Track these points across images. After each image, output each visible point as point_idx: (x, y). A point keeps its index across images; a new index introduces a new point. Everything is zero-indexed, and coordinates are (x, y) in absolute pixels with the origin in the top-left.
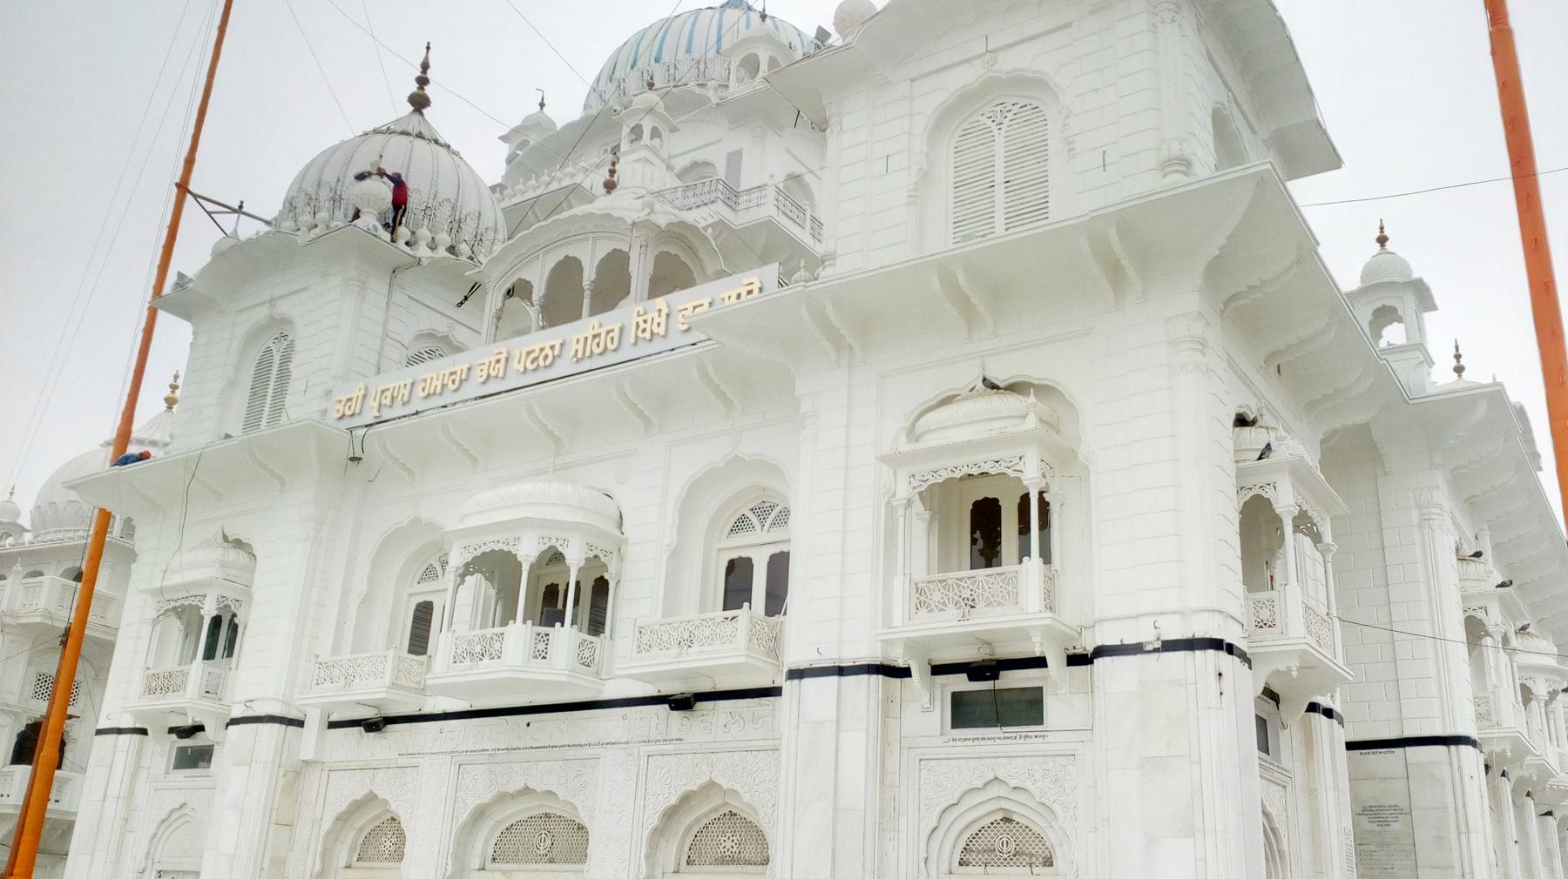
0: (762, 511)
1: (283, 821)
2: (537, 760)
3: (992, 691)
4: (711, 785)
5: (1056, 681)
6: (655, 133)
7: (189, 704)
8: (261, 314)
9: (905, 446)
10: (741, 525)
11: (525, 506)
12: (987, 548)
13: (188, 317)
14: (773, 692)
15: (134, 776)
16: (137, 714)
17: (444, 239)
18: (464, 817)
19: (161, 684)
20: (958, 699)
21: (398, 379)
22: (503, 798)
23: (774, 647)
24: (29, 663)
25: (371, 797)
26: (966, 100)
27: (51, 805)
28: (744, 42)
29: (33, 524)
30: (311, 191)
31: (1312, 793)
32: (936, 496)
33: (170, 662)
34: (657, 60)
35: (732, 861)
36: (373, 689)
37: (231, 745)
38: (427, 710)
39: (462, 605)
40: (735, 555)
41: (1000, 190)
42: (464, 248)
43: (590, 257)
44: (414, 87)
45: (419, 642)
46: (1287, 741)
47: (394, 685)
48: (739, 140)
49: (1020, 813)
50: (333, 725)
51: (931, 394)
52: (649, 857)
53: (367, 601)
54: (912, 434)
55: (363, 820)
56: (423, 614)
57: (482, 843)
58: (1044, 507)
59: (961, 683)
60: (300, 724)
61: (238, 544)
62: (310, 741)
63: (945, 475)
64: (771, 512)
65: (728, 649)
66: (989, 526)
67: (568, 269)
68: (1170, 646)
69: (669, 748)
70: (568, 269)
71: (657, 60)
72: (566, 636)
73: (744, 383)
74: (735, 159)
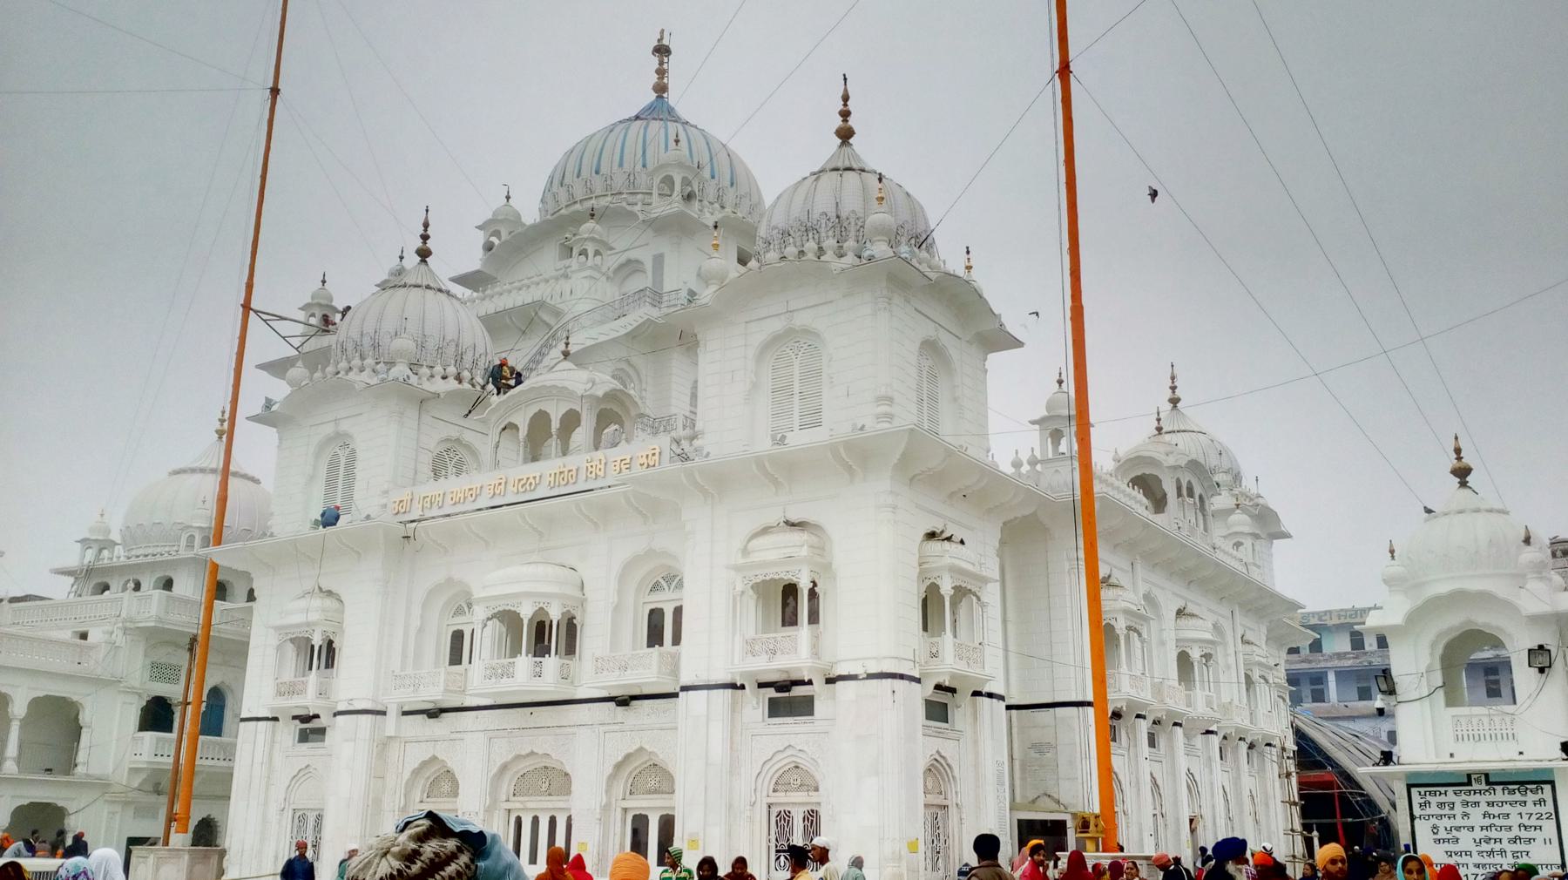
0: (670, 579)
1: (378, 775)
2: (543, 737)
3: (787, 698)
4: (641, 749)
5: (818, 688)
6: (597, 253)
7: (308, 701)
8: (329, 429)
9: (741, 561)
10: (656, 587)
11: (520, 580)
14: (675, 695)
15: (272, 748)
16: (272, 709)
17: (452, 370)
18: (495, 770)
22: (518, 757)
23: (675, 671)
24: (145, 656)
25: (434, 758)
26: (775, 340)
28: (661, 167)
29: (123, 538)
30: (356, 337)
31: (976, 742)
32: (762, 589)
33: (288, 675)
34: (597, 172)
35: (656, 792)
36: (432, 694)
38: (467, 704)
39: (486, 641)
41: (796, 398)
42: (466, 374)
43: (556, 413)
44: (419, 243)
45: (456, 658)
46: (1162, 741)
47: (446, 691)
48: (663, 245)
50: (405, 713)
51: (758, 526)
53: (421, 630)
54: (745, 551)
55: (429, 772)
56: (458, 637)
57: (506, 787)
58: (813, 594)
59: (771, 693)
60: (384, 713)
61: (330, 593)
62: (391, 724)
63: (761, 578)
64: (673, 579)
65: (647, 671)
66: (790, 603)
67: (541, 419)
68: (871, 676)
70: (541, 419)
71: (597, 172)
72: (551, 662)
73: (650, 506)
74: (659, 260)
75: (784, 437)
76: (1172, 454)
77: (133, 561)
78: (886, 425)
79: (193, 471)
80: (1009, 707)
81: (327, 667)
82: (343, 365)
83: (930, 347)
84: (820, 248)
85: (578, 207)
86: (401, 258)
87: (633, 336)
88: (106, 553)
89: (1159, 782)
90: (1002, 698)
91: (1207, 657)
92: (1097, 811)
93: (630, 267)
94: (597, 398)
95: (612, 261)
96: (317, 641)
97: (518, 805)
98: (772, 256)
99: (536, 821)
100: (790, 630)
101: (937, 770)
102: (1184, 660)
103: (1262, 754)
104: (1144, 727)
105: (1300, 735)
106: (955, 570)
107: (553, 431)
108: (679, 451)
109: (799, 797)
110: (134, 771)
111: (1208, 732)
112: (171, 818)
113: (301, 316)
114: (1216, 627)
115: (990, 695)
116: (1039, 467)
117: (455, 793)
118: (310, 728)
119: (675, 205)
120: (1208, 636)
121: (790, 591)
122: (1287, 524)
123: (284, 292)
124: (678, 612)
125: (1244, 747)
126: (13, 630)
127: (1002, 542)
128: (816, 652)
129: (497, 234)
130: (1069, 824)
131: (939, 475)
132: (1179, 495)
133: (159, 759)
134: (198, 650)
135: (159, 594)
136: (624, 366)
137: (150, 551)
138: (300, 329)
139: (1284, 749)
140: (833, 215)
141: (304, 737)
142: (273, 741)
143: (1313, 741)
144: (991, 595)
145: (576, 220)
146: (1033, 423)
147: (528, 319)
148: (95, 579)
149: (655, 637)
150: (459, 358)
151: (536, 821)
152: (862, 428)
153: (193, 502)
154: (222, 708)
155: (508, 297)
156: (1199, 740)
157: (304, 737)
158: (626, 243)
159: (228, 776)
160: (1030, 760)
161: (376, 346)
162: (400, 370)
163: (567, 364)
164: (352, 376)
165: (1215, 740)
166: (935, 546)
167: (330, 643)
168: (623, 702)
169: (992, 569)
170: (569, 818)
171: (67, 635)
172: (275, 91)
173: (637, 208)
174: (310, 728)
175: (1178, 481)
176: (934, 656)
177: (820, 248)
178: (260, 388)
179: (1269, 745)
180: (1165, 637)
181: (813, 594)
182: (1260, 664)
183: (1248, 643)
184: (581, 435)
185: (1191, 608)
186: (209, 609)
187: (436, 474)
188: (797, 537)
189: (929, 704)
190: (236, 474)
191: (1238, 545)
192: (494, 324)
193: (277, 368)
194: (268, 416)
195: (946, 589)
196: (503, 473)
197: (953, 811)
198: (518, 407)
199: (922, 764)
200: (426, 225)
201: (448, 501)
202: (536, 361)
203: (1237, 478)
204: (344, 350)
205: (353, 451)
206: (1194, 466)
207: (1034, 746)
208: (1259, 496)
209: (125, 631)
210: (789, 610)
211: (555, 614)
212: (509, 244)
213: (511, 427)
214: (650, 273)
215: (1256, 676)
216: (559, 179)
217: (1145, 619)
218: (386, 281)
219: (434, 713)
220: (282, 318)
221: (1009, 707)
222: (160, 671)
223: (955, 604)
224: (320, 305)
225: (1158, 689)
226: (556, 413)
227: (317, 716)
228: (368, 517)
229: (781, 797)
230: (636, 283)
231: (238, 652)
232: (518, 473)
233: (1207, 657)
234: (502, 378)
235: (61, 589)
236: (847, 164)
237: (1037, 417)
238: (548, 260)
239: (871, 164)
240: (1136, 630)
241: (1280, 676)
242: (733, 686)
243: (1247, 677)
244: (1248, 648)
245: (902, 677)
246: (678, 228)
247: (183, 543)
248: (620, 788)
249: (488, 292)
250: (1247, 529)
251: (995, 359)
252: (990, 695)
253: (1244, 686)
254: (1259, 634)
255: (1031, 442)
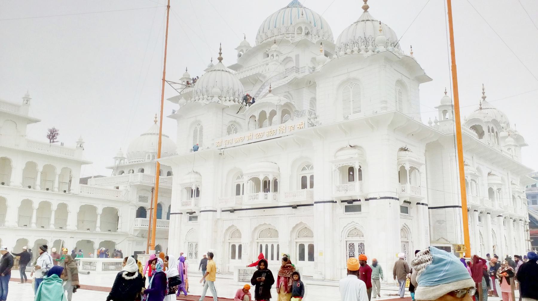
0: (308, 166)
3: (352, 205)
5: (363, 203)
6: (277, 55)
7: (192, 207)
10: (304, 169)
12: (351, 178)
13: (176, 119)
14: (312, 205)
17: (232, 98)
18: (253, 229)
19: (184, 204)
20: (346, 207)
21: (229, 138)
22: (260, 225)
23: (312, 197)
25: (233, 226)
27: (157, 227)
30: (201, 89)
32: (341, 169)
34: (275, 27)
35: (307, 237)
37: (202, 216)
38: (243, 208)
39: (248, 187)
40: (303, 175)
41: (351, 103)
42: (236, 99)
43: (268, 112)
44: (218, 56)
46: (483, 219)
49: (357, 227)
50: (223, 211)
52: (291, 236)
55: (299, 227)
56: (238, 186)
57: (257, 235)
58: (360, 170)
59: (346, 204)
61: (197, 173)
62: (219, 214)
63: (342, 165)
64: (309, 166)
65: (302, 197)
68: (381, 198)
69: (293, 215)
71: (275, 27)
72: (270, 194)
74: (297, 56)
75: (348, 116)
76: (485, 117)
77: (131, 163)
78: (385, 111)
79: (148, 134)
80: (429, 208)
81: (197, 196)
82: (197, 98)
83: (400, 82)
84: (359, 49)
85: (269, 40)
86: (212, 61)
87: (290, 83)
88: (122, 161)
89: (482, 233)
90: (427, 205)
91: (499, 189)
92: (464, 243)
93: (287, 60)
94: (282, 106)
95: (282, 58)
96: (194, 188)
97: (261, 241)
98: (342, 53)
99: (272, 246)
100: (351, 183)
101: (405, 229)
102: (491, 191)
103: (518, 223)
104: (477, 214)
105: (531, 217)
106: (410, 161)
107: (267, 117)
108: (310, 123)
109: (357, 238)
110: (135, 230)
111: (499, 216)
112: (149, 245)
113: (180, 82)
114: (502, 179)
115: (423, 204)
116: (438, 124)
117: (240, 237)
118: (192, 216)
119: (302, 37)
120: (500, 182)
121: (351, 169)
122: (526, 141)
123: (175, 74)
124: (312, 177)
125: (512, 221)
126: (96, 186)
127: (426, 151)
128: (361, 190)
129: (242, 51)
130: (452, 248)
131: (406, 129)
132: (489, 132)
133: (143, 226)
134: (155, 192)
135: (140, 174)
136: (287, 94)
137: (136, 160)
138: (180, 86)
139: (526, 222)
140: (363, 37)
141: (190, 219)
142: (181, 221)
143: (535, 218)
144: (422, 169)
145: (269, 44)
146: (436, 108)
147: (254, 80)
148: (120, 170)
149: (304, 186)
150: (234, 94)
151: (272, 246)
152: (376, 112)
153: (149, 144)
154: (161, 210)
155: (246, 73)
156: (496, 219)
157: (190, 219)
158: (286, 51)
159: (167, 232)
160: (437, 226)
161: (207, 91)
162: (216, 99)
163: (270, 94)
164: (200, 101)
165: (502, 219)
166: (404, 153)
167: (198, 189)
168: (295, 207)
169: (422, 160)
170: (278, 245)
171: (112, 188)
172: (169, 7)
173: (289, 39)
174: (192, 216)
175: (489, 127)
176: (403, 191)
177: (359, 49)
178: (170, 107)
179: (521, 220)
180: (484, 183)
181: (360, 170)
182: (518, 192)
183: (514, 184)
184: (277, 118)
185: (493, 172)
186: (158, 178)
187: (229, 132)
188: (353, 151)
189: (401, 207)
190: (164, 135)
191: (509, 149)
192: (244, 82)
193: (175, 100)
194: (174, 115)
195: (407, 168)
196: (249, 132)
197: (410, 243)
198: (254, 110)
199: (400, 227)
200: (221, 50)
201: (234, 142)
202: (258, 94)
203: (508, 125)
204: (197, 93)
205: (202, 126)
206: (495, 121)
207: (438, 221)
208: (516, 131)
209: (130, 186)
210: (351, 176)
211: (271, 179)
212: (246, 54)
213: (253, 116)
214: (294, 61)
215: (516, 196)
216: (262, 30)
217: (477, 176)
218: (207, 69)
219: (232, 211)
220: (175, 83)
221: (429, 208)
222: (142, 199)
223: (410, 172)
224: (186, 78)
225: (482, 201)
226: (268, 112)
227: (195, 212)
228: (208, 148)
229: (350, 239)
230: (290, 65)
231: (168, 192)
232: (256, 133)
233: (499, 189)
234: (248, 100)
235: (109, 173)
236: (367, 19)
237: (437, 106)
238: (260, 59)
239: (375, 18)
240: (474, 181)
241: (524, 196)
242: (333, 202)
243: (513, 196)
244: (513, 186)
245: (393, 198)
246: (303, 45)
247: (147, 157)
248: (295, 235)
249: (241, 71)
250: (513, 144)
251: (422, 86)
252: (423, 204)
253: (512, 200)
254: (517, 181)
255: (436, 115)
